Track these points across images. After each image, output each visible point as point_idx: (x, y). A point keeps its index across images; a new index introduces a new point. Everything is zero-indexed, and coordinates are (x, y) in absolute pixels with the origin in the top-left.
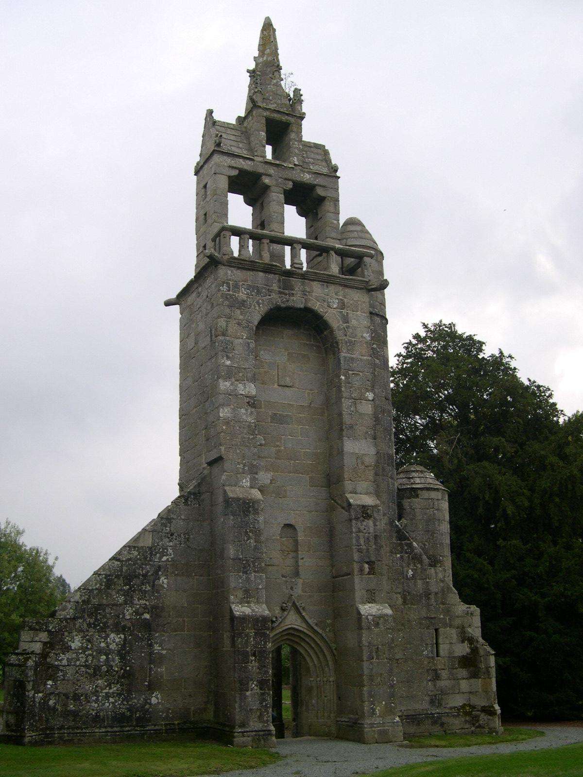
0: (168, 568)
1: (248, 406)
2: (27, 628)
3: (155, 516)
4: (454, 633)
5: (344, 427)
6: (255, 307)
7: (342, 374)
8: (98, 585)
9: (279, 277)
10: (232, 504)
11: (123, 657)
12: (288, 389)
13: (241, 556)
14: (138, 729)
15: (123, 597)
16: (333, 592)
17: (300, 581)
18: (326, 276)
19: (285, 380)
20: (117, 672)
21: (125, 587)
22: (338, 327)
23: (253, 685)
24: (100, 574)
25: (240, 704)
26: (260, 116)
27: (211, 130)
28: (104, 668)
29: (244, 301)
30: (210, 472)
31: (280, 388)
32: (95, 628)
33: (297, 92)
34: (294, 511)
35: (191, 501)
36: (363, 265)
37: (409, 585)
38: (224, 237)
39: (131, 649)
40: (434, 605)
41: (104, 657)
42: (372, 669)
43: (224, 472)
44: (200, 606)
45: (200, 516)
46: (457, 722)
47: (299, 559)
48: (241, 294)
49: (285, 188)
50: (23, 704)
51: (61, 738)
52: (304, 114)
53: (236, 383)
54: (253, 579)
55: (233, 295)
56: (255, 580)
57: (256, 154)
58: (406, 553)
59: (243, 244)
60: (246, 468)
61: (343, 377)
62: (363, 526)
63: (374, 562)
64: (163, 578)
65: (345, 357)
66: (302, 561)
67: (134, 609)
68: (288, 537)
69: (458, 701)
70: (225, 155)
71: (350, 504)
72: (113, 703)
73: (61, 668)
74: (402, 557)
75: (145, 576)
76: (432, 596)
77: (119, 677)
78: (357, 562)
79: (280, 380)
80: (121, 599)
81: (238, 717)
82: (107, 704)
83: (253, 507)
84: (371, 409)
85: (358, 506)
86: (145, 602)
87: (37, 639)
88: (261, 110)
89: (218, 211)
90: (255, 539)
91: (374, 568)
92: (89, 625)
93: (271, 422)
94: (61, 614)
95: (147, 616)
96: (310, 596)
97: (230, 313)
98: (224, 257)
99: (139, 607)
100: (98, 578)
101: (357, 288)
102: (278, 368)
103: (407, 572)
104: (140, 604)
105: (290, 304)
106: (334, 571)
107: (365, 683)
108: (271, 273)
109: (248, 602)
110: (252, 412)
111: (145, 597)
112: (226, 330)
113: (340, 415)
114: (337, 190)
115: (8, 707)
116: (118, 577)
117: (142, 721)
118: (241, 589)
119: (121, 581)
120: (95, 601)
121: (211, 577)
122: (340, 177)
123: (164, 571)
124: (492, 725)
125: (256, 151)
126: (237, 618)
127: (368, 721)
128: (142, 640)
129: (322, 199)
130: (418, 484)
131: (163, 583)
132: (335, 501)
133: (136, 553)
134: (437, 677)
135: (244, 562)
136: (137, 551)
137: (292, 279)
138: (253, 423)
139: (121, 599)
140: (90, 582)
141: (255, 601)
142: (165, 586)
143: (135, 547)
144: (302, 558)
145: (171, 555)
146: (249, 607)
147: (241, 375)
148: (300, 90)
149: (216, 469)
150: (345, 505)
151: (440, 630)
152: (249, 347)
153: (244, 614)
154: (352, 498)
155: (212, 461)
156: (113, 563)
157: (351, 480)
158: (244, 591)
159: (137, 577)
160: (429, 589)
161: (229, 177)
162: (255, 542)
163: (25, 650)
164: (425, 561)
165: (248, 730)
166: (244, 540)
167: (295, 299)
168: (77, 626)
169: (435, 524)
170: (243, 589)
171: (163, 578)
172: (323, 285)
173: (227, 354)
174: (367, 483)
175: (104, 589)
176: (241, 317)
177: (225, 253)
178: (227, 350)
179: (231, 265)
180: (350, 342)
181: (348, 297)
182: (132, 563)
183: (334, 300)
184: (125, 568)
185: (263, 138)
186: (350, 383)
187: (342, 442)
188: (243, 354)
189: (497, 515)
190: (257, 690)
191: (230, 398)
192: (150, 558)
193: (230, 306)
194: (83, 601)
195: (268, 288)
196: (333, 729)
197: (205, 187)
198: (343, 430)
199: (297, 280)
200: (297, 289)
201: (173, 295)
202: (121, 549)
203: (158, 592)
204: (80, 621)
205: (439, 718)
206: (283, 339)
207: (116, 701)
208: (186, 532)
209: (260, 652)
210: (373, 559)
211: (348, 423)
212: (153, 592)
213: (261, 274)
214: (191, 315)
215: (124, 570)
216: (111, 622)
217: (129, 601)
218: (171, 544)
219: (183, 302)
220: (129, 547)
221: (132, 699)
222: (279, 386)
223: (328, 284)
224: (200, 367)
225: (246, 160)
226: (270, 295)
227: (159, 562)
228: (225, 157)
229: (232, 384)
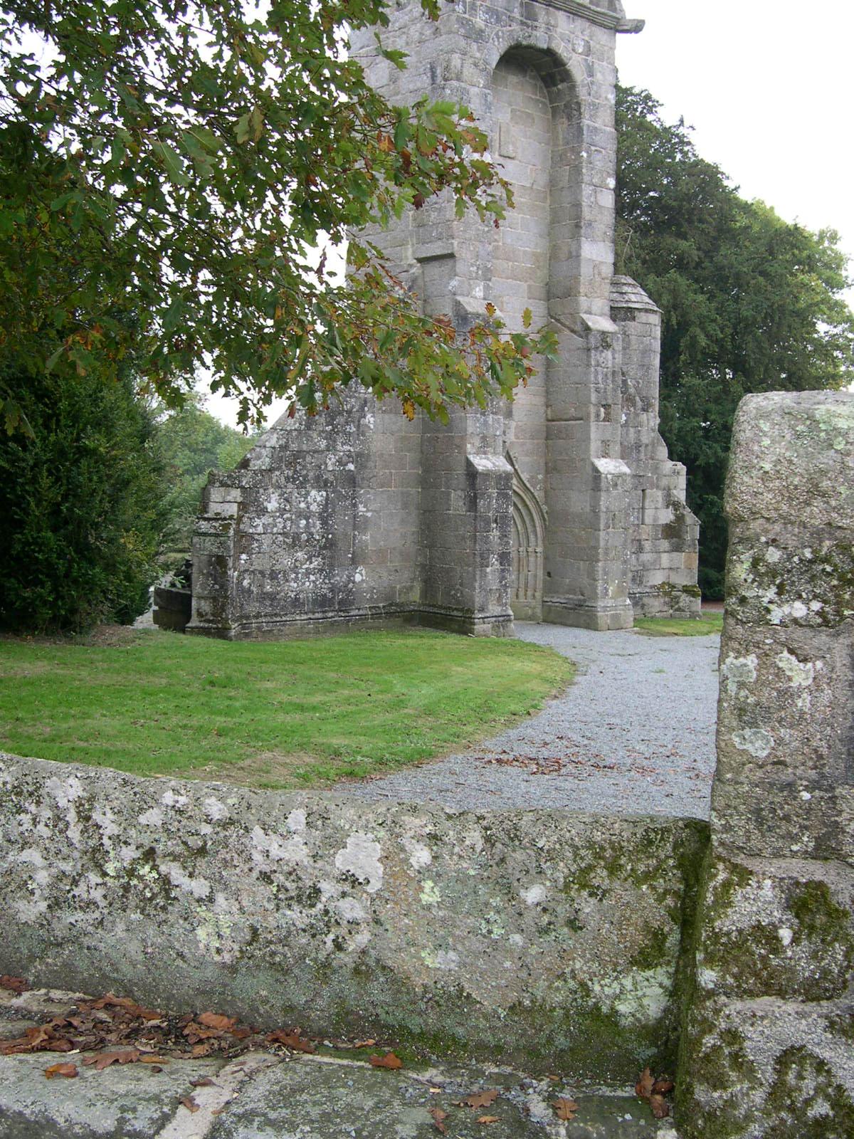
2: (217, 484)
4: (659, 495)
11: (324, 522)
14: (342, 614)
16: (547, 438)
17: (513, 424)
22: (583, 81)
23: (494, 559)
28: (304, 537)
29: (482, 31)
32: (293, 483)
39: (333, 510)
41: (303, 522)
42: (607, 541)
46: (656, 603)
50: (224, 587)
51: (259, 628)
54: (490, 422)
69: (657, 578)
71: (588, 329)
72: (314, 582)
73: (256, 537)
75: (349, 412)
76: (642, 449)
77: (320, 547)
80: (323, 444)
81: (478, 601)
82: (307, 584)
85: (599, 331)
86: (349, 448)
87: (229, 498)
92: (287, 478)
94: (255, 465)
95: (351, 467)
96: (523, 444)
101: (605, 27)
105: (532, 41)
106: (549, 412)
107: (601, 557)
109: (485, 453)
113: (577, 205)
115: (200, 591)
117: (345, 605)
120: (294, 447)
124: (694, 609)
126: (481, 474)
127: (600, 604)
128: (345, 498)
132: (558, 320)
134: (640, 549)
139: (323, 444)
142: (372, 426)
146: (488, 459)
149: (434, 270)
150: (578, 328)
152: (486, 100)
163: (219, 514)
165: (488, 615)
168: (274, 481)
171: (369, 416)
176: (478, 55)
187: (580, 247)
190: (497, 566)
193: (466, 37)
194: (281, 446)
196: (539, 611)
200: (540, 20)
204: (277, 473)
205: (640, 598)
207: (317, 580)
209: (501, 517)
210: (610, 402)
211: (587, 218)
216: (311, 474)
221: (334, 576)
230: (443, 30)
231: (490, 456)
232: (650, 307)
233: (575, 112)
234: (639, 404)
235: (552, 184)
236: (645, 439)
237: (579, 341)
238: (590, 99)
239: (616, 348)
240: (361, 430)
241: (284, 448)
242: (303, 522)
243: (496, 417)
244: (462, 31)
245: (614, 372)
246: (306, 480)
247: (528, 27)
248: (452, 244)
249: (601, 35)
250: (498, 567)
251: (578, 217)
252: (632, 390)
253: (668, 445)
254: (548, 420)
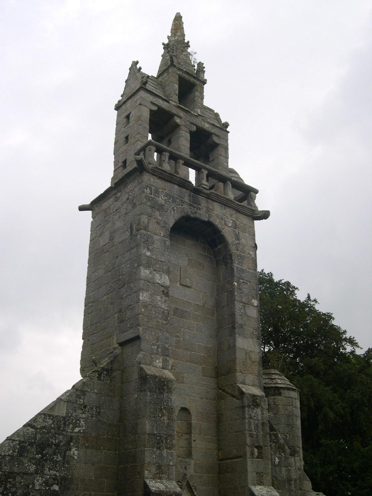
0: (79, 439)
1: (163, 295)
3: (70, 388)
5: (236, 325)
6: (171, 212)
7: (235, 280)
8: (11, 451)
9: (190, 193)
10: (150, 381)
12: (187, 288)
13: (156, 432)
15: (34, 466)
16: (219, 473)
17: (193, 462)
18: (225, 199)
19: (186, 281)
21: (37, 456)
22: (232, 242)
24: (14, 440)
26: (175, 73)
27: (137, 74)
30: (122, 352)
31: (181, 287)
33: (200, 65)
34: (189, 396)
35: (104, 377)
36: (250, 198)
37: (276, 472)
38: (150, 151)
40: (294, 490)
43: (140, 351)
44: (106, 480)
45: (111, 392)
47: (192, 440)
48: (160, 199)
49: (191, 129)
52: (206, 80)
53: (154, 272)
54: (165, 455)
55: (154, 198)
56: (167, 457)
57: (171, 99)
59: (164, 160)
61: (236, 284)
62: (254, 414)
63: (262, 447)
64: (74, 449)
65: (237, 267)
66: (194, 443)
67: (44, 480)
68: (182, 420)
70: (149, 94)
71: (242, 393)
75: (57, 445)
76: (293, 482)
78: (249, 446)
79: (182, 280)
80: (33, 468)
83: (167, 386)
84: (256, 314)
85: (250, 395)
88: (176, 69)
89: (142, 133)
90: (168, 416)
91: (262, 452)
93: (173, 315)
95: (56, 487)
97: (151, 212)
98: (149, 165)
99: (49, 478)
100: (12, 444)
101: (246, 215)
102: (180, 270)
103: (275, 459)
104: (51, 475)
105: (197, 216)
108: (184, 188)
109: (160, 478)
110: (166, 300)
111: (56, 467)
112: (148, 226)
113: (233, 315)
114: (227, 140)
116: (31, 444)
118: (154, 464)
119: (33, 450)
121: (117, 452)
122: (229, 132)
123: (76, 442)
125: (172, 97)
126: (153, 493)
129: (216, 145)
130: (280, 384)
131: (74, 454)
132: (224, 391)
133: (50, 422)
135: (158, 438)
136: (52, 419)
137: (200, 196)
138: (166, 310)
139: (33, 468)
140: (4, 448)
141: (167, 477)
142: (76, 457)
143: (50, 416)
144: (195, 441)
145: (83, 427)
146: (162, 483)
147: (158, 266)
148: (203, 64)
149: (129, 349)
150: (236, 393)
152: (165, 244)
153: (159, 489)
154: (243, 387)
155: (134, 337)
156: (28, 430)
157: (241, 372)
158: (158, 466)
159: (49, 446)
160: (290, 476)
161: (151, 111)
162: (168, 419)
164: (287, 451)
166: (159, 416)
167: (201, 213)
169: (293, 419)
170: (157, 464)
171: (74, 449)
172: (222, 206)
173: (148, 246)
174: (253, 376)
175: (17, 456)
176: (160, 218)
177: (150, 162)
178: (148, 242)
179: (154, 173)
180: (241, 256)
181: (238, 220)
182: (46, 431)
183: (230, 221)
184: (39, 436)
185: (176, 89)
186: (240, 289)
187: (235, 340)
188: (160, 249)
189: (319, 419)
191: (149, 285)
192: (63, 428)
193: (152, 207)
195: (181, 199)
197: (128, 117)
198: (236, 328)
199: (203, 198)
200: (203, 205)
201: (88, 202)
202: (36, 416)
203: (68, 463)
206: (184, 246)
208: (98, 406)
210: (261, 444)
211: (239, 322)
212: (64, 463)
213: (176, 187)
214: (105, 217)
215: (37, 438)
217: (39, 471)
218: (84, 416)
219: (96, 208)
220: (44, 414)
222: (181, 285)
223: (225, 207)
224: (115, 259)
225: (164, 101)
226: (182, 205)
227: (72, 433)
228: (149, 95)
229: (151, 273)
230: (137, 203)
231: (164, 481)
232: (291, 387)
233: (229, 260)
234: (288, 451)
235: (218, 305)
236: (294, 475)
237: (237, 402)
238: (238, 253)
239: (264, 407)
240: (66, 460)
243: (169, 451)
244: (149, 203)
245: (263, 424)
247: (195, 207)
248: (138, 329)
249: (244, 220)
251: (234, 322)
252: (282, 441)
253: (312, 479)
254: (220, 460)
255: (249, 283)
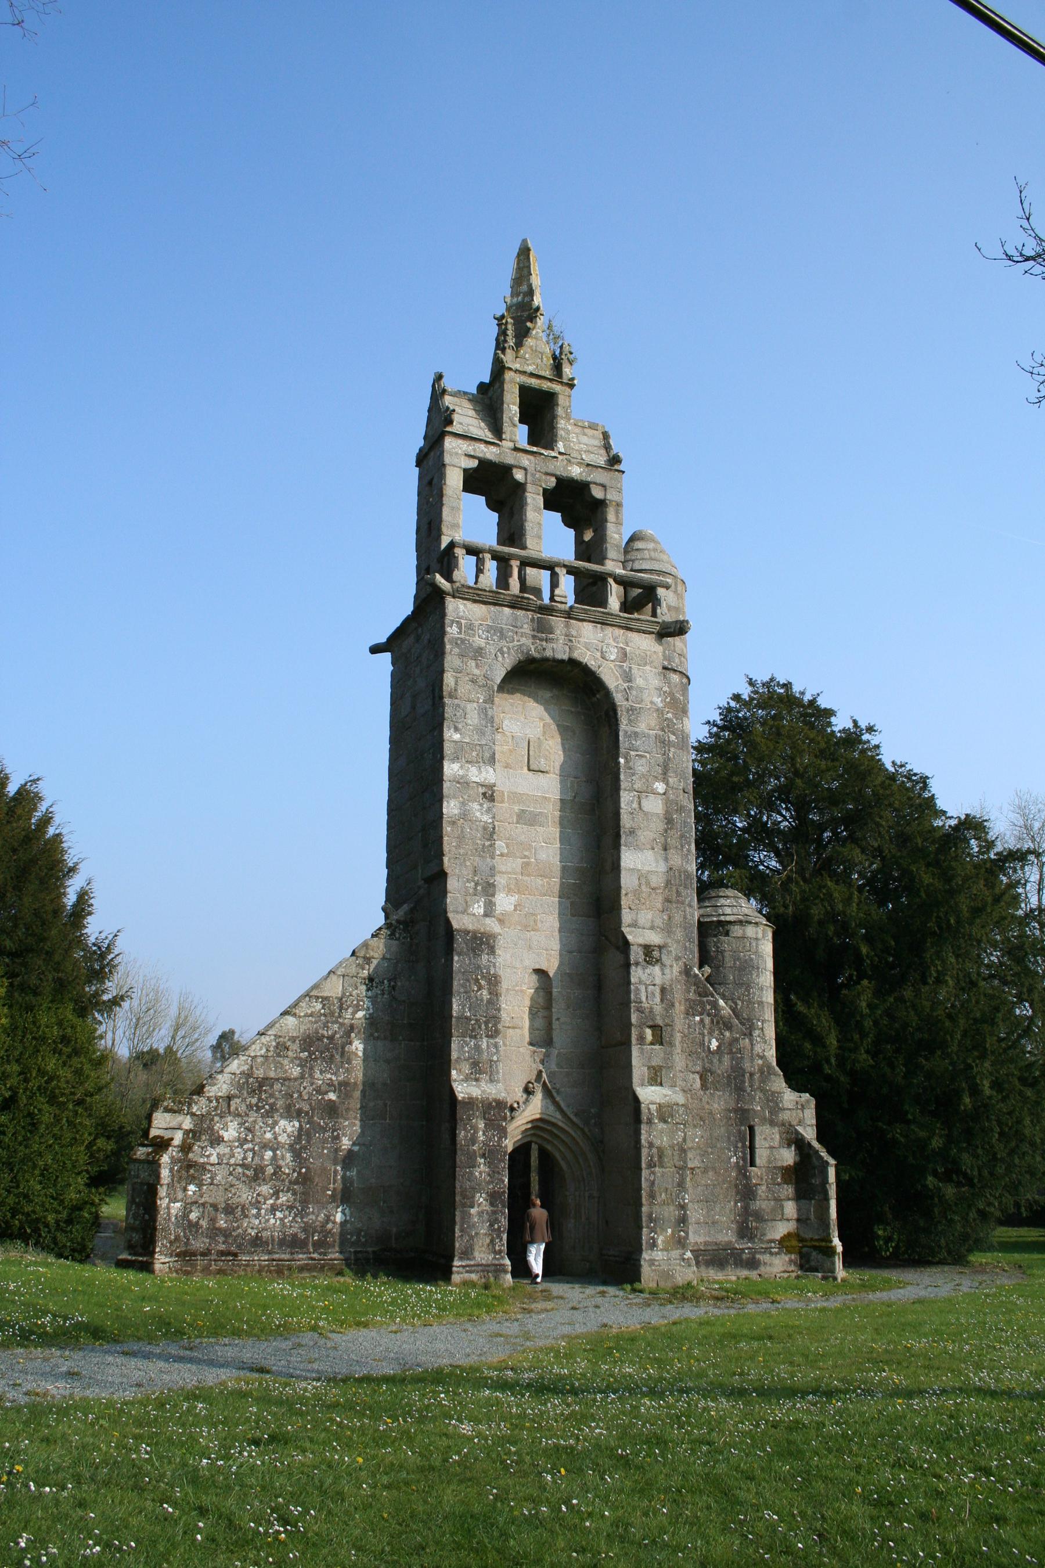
20: (288, 1175)
25: (462, 1226)
28: (270, 1170)
31: (531, 773)
34: (547, 950)
54: (484, 1046)
58: (709, 1015)
60: (479, 888)
72: (281, 1219)
73: (209, 1167)
74: (702, 1020)
75: (331, 1038)
77: (290, 1182)
80: (296, 1072)
82: (272, 1221)
86: (329, 1076)
90: (489, 989)
92: (250, 1107)
93: (517, 823)
95: (332, 1096)
101: (644, 632)
105: (549, 653)
109: (477, 1080)
118: (467, 1060)
120: (260, 1073)
127: (646, 1255)
128: (324, 1130)
139: (296, 1072)
146: (478, 1087)
151: (756, 1128)
176: (477, 672)
201: (383, 639)
204: (238, 1101)
207: (285, 1217)
210: (660, 1022)
211: (628, 826)
213: (507, 610)
216: (280, 1103)
221: (308, 1214)
241: (248, 1075)
242: (269, 1154)
246: (273, 1109)
250: (488, 1208)
255: (648, 755)
